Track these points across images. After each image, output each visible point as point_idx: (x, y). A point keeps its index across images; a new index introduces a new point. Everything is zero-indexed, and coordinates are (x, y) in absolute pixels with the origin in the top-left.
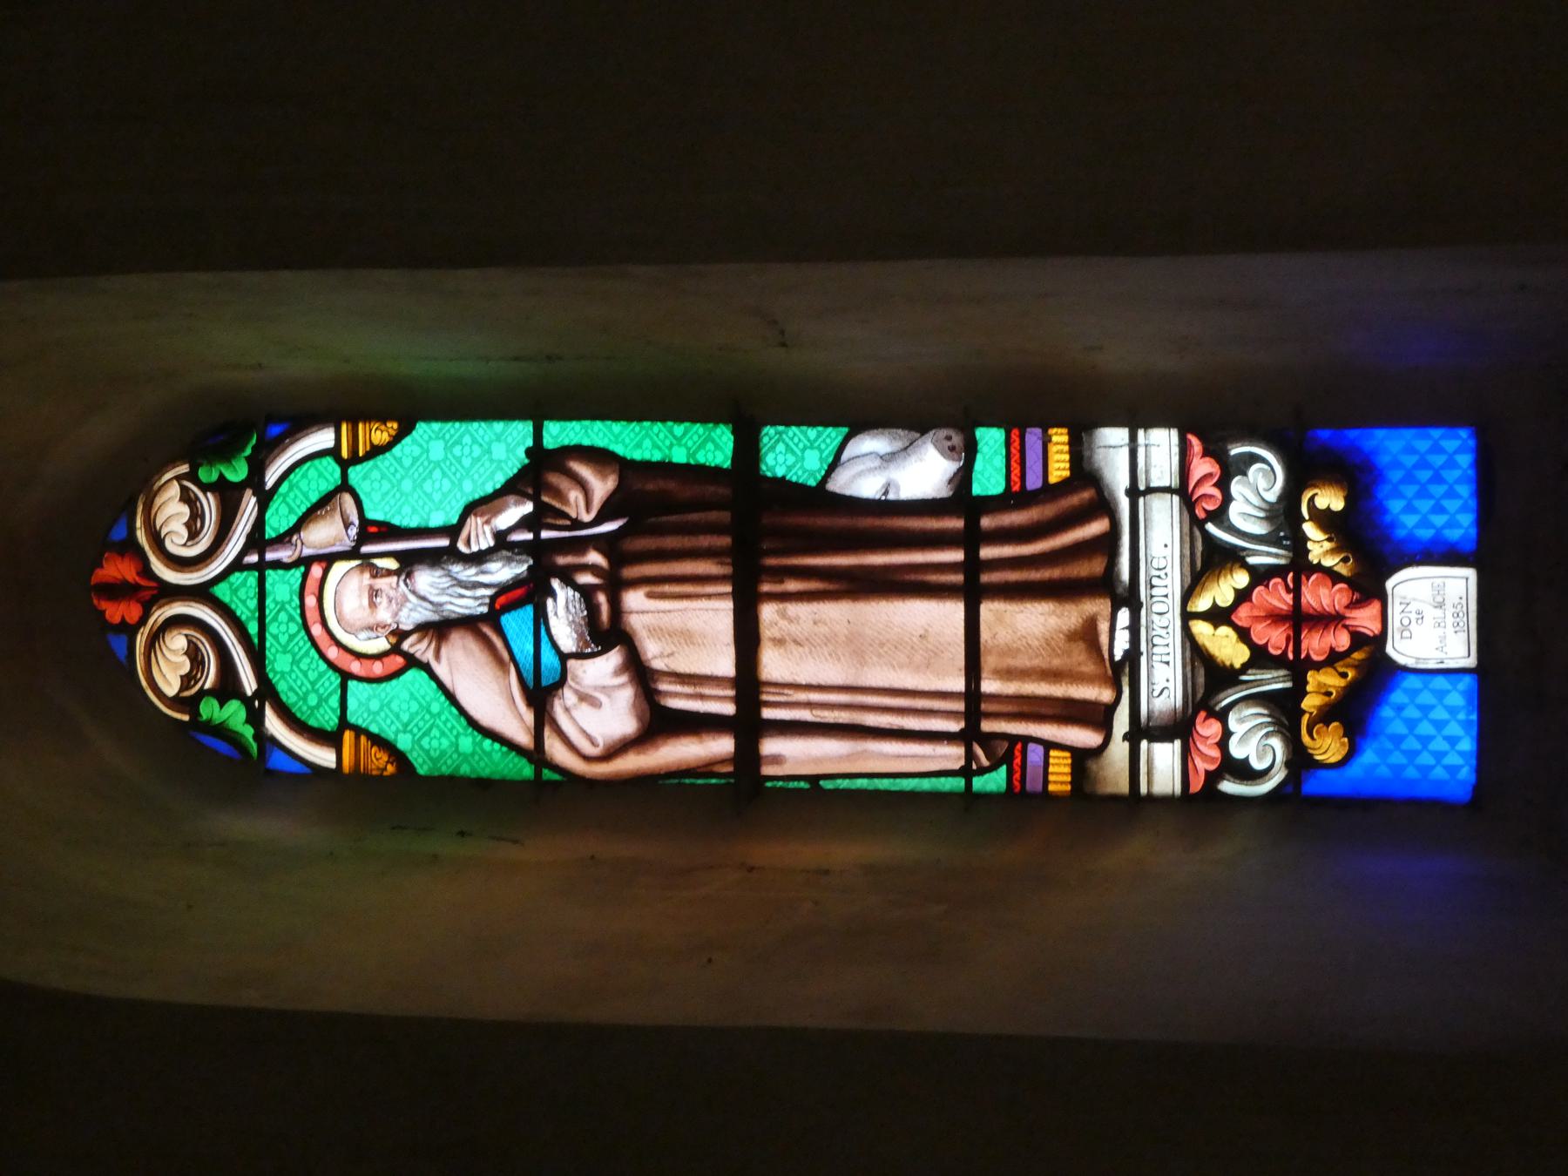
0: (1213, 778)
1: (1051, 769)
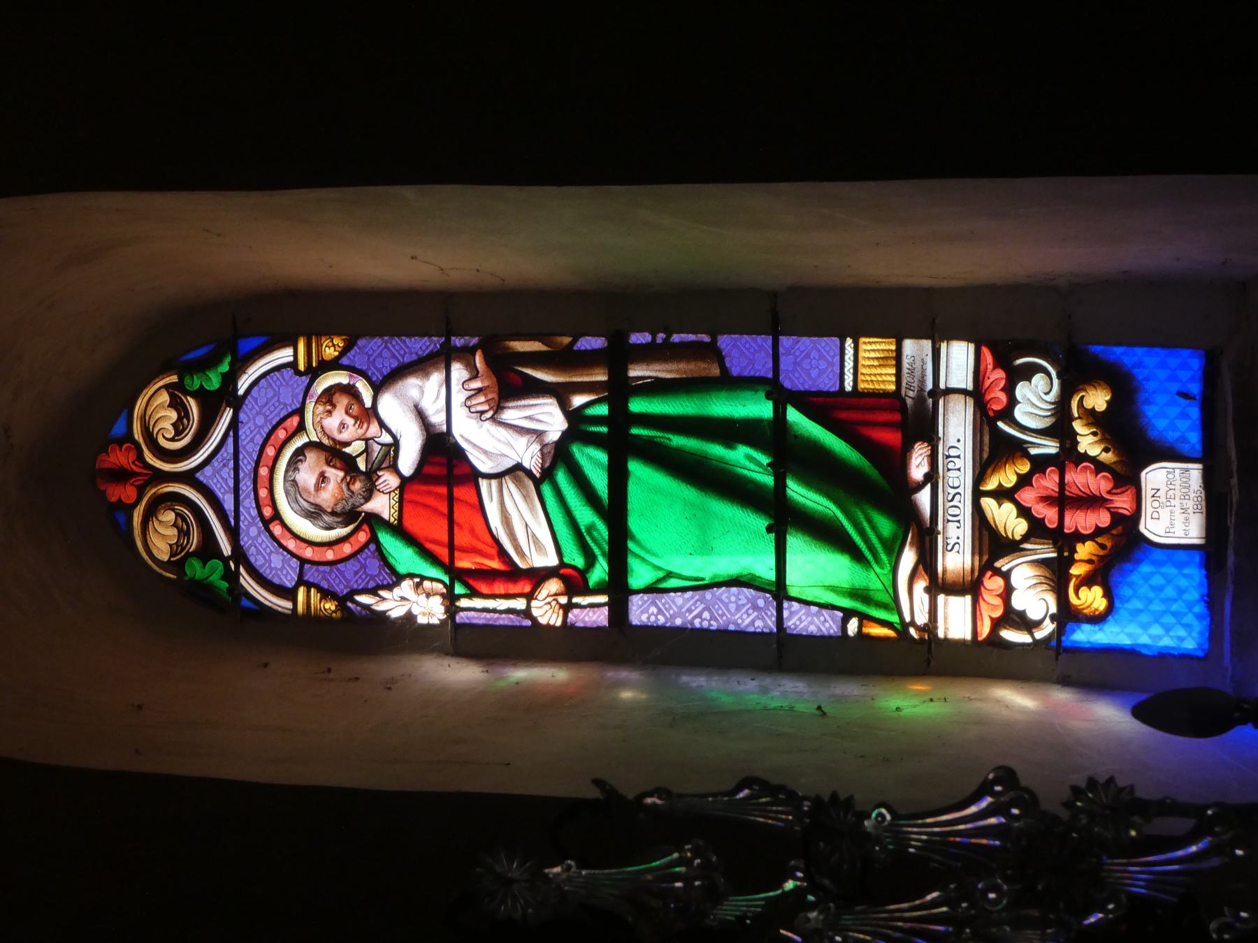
0: (997, 624)
1: (893, 371)
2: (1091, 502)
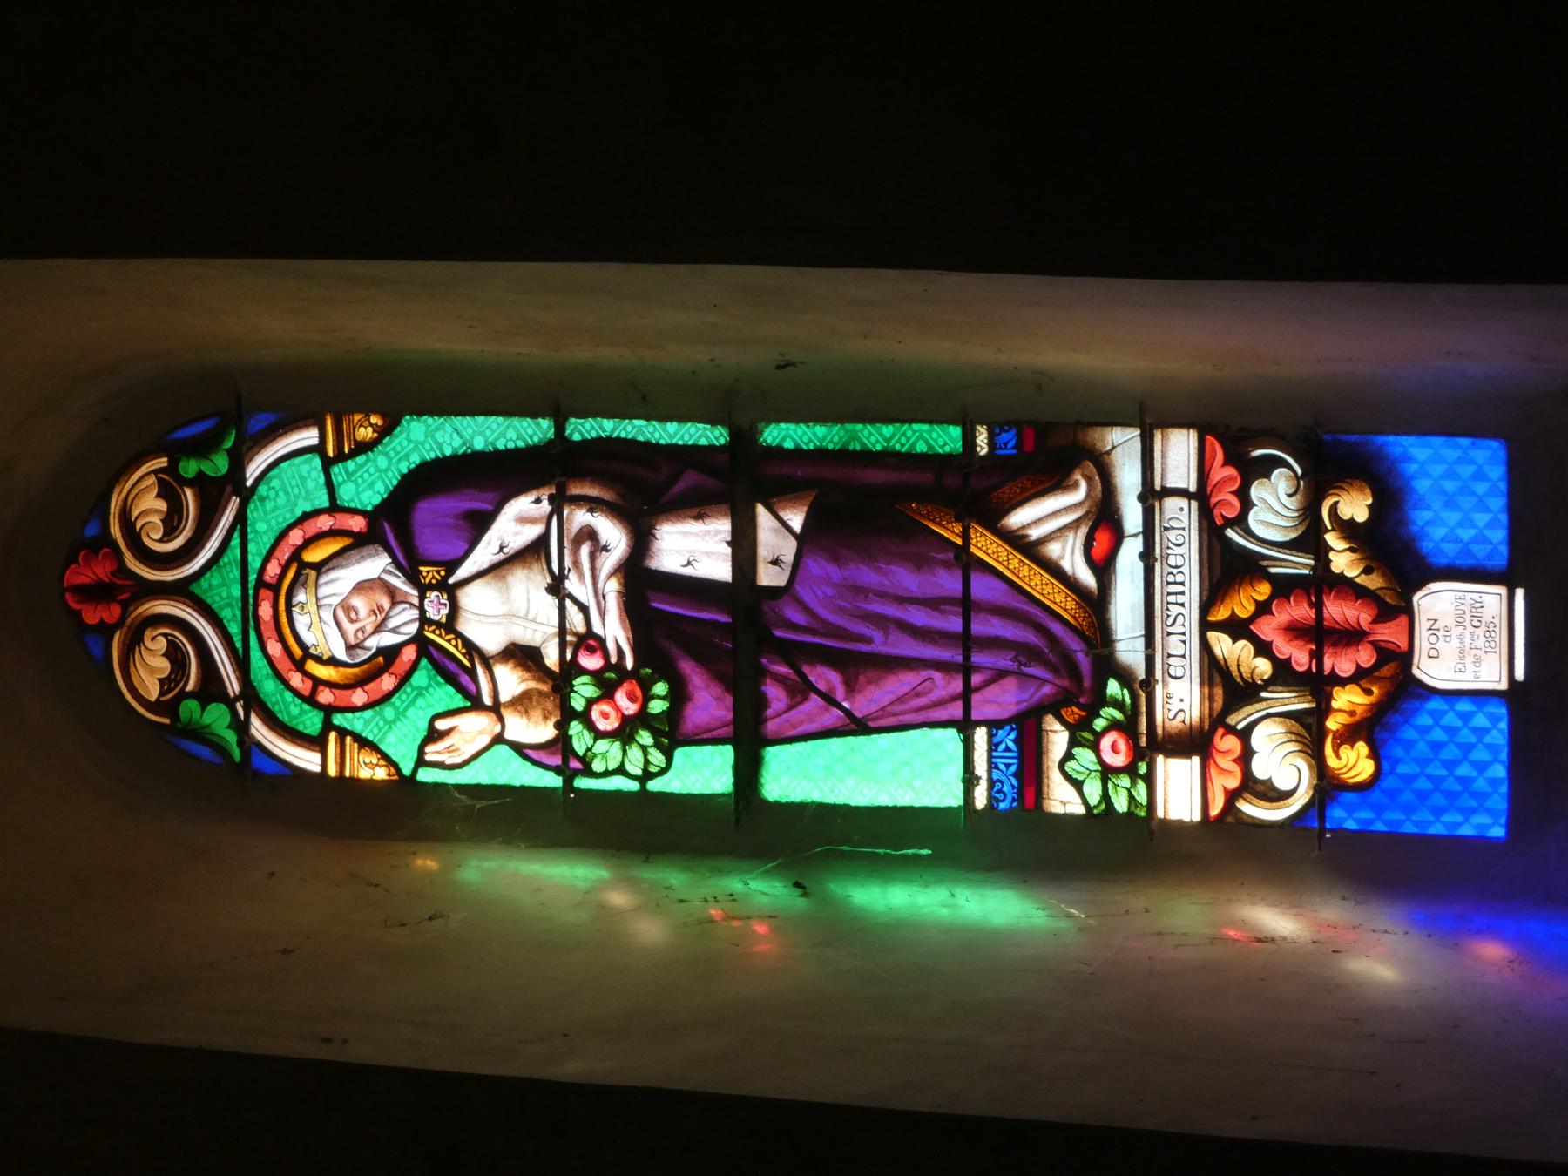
0: (1232, 796)
2: (1350, 637)
